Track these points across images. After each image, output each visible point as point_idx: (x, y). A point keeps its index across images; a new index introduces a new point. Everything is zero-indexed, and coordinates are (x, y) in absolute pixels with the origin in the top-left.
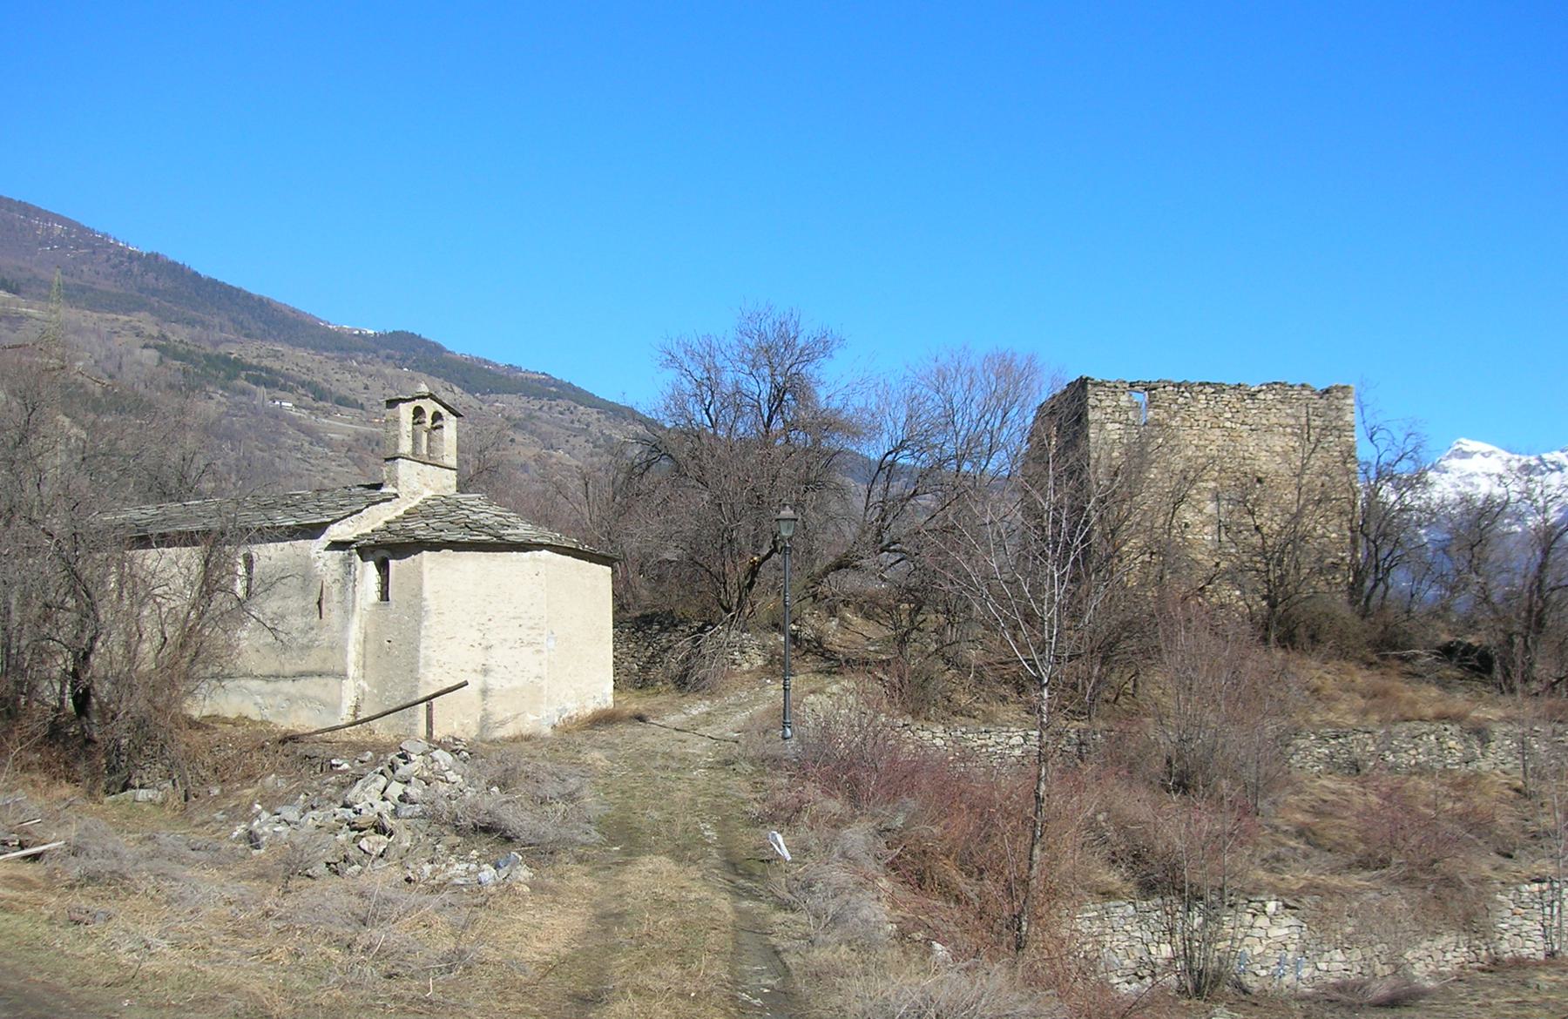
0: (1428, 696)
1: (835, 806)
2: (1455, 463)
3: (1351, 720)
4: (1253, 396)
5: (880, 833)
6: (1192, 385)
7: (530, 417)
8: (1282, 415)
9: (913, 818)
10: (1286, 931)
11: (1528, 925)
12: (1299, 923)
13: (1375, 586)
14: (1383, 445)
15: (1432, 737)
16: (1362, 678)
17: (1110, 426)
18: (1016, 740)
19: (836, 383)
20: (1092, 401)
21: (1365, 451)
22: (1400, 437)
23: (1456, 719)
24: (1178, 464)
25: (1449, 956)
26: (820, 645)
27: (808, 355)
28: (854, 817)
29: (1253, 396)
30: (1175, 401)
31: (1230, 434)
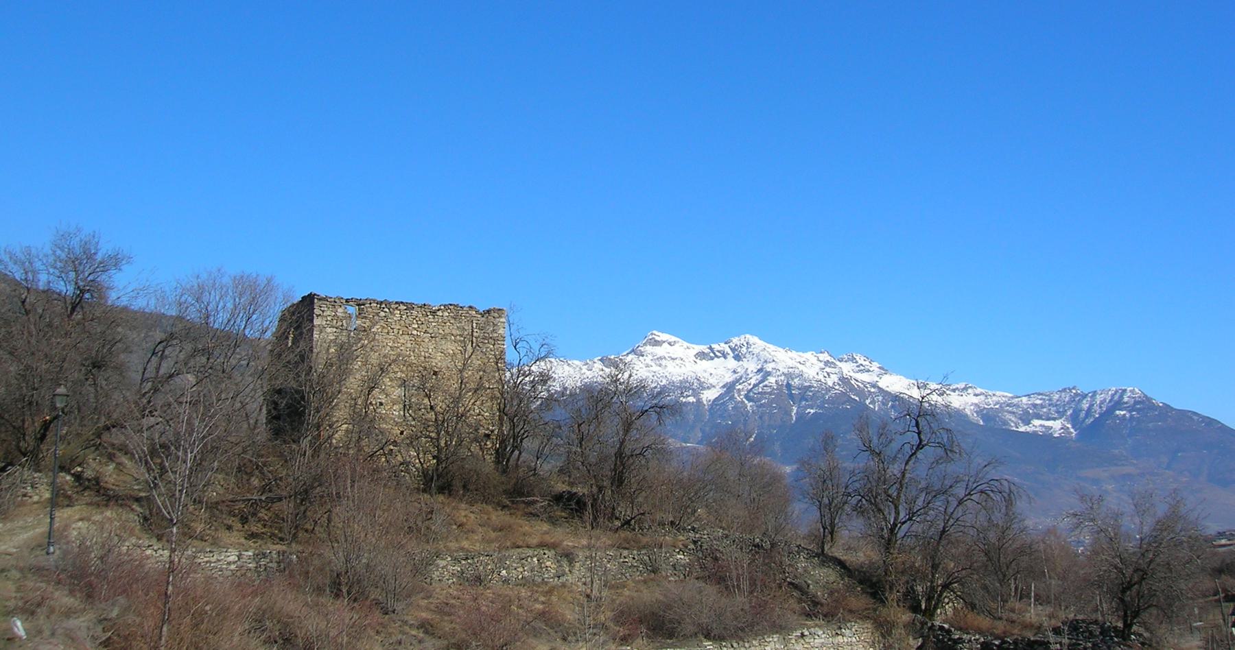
0: (539, 529)
1: (68, 601)
2: (649, 348)
3: (478, 547)
4: (434, 313)
5: (100, 621)
6: (390, 303)
8: (452, 328)
9: (126, 610)
16: (498, 517)
17: (329, 330)
18: (233, 558)
20: (317, 311)
21: (511, 356)
22: (536, 347)
23: (552, 546)
24: (374, 358)
26: (98, 483)
27: (104, 267)
28: (85, 610)
29: (434, 313)
30: (377, 314)
31: (417, 340)
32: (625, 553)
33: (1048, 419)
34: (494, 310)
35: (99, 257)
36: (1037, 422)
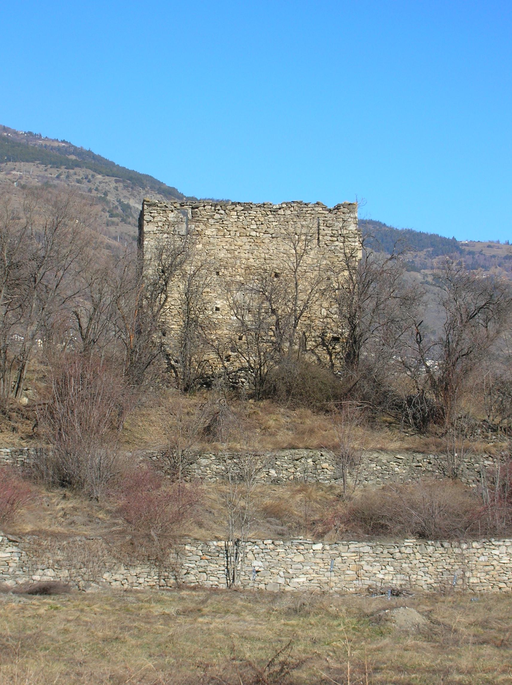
7: (47, 185)
10: (9, 555)
11: (212, 567)
12: (20, 550)
15: (310, 460)
25: (141, 580)
30: (212, 217)
32: (419, 457)
34: (344, 206)
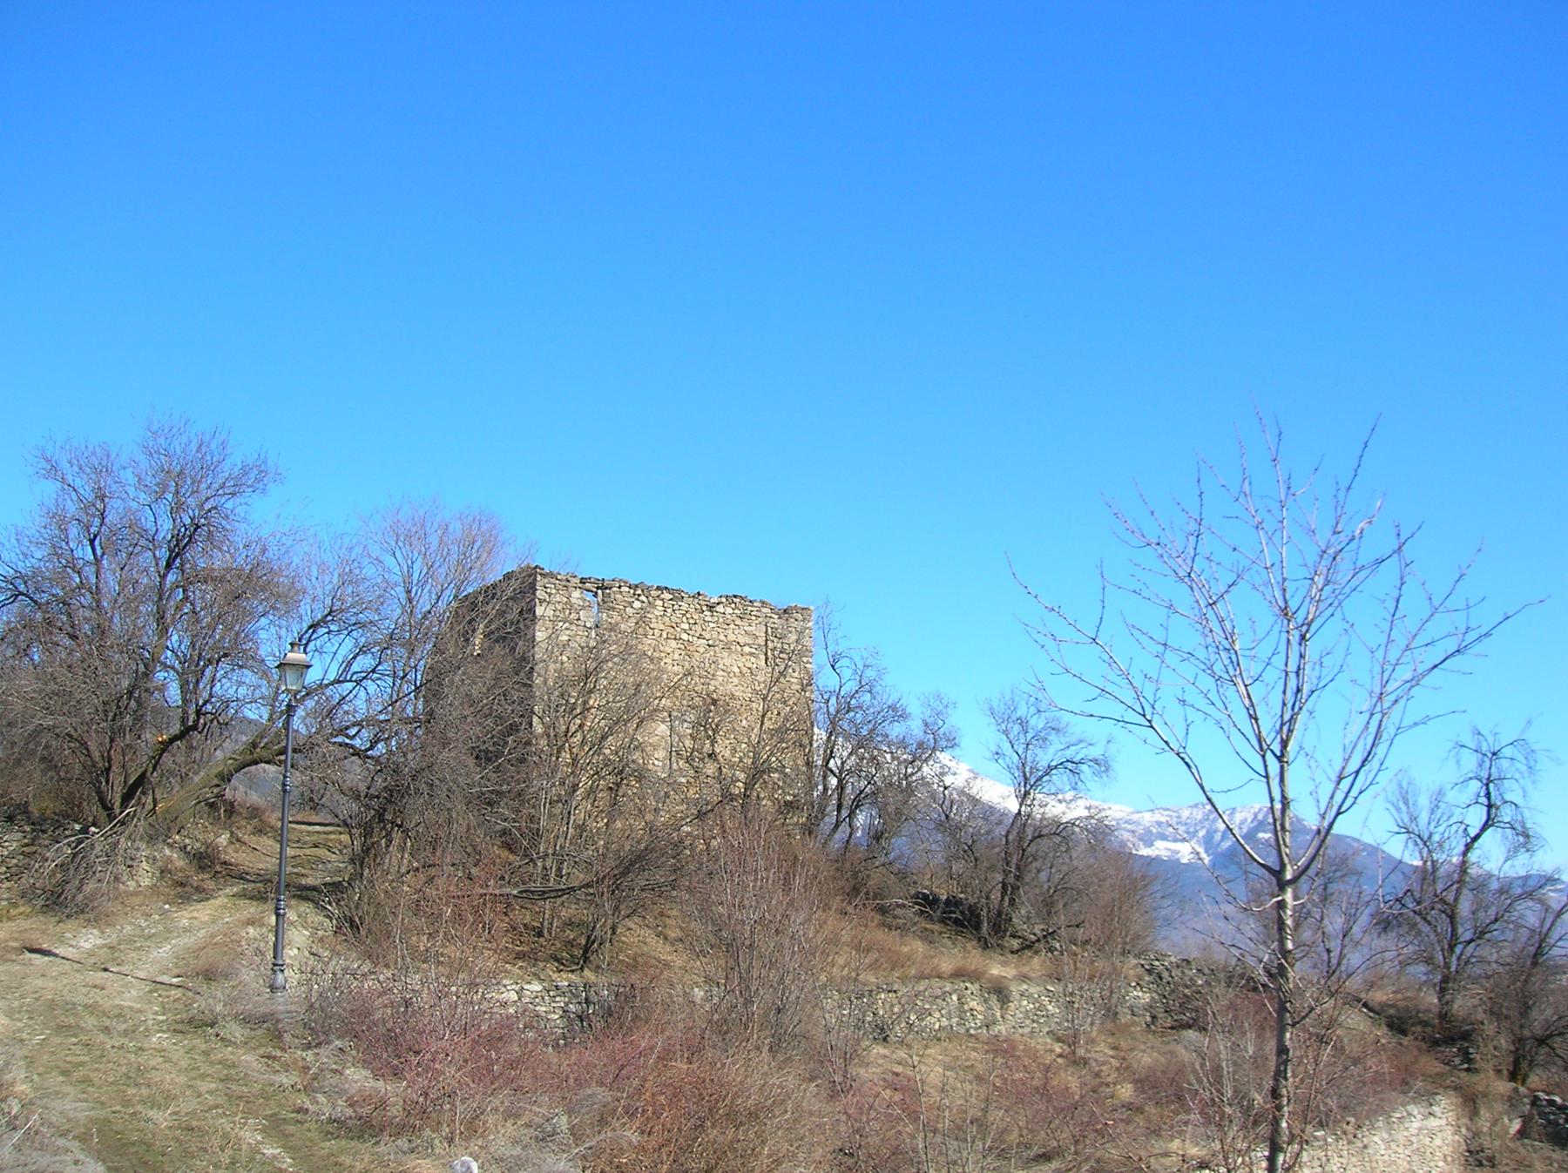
4: (711, 608)
13: (837, 826)
14: (847, 674)
15: (955, 997)
19: (260, 522)
20: (540, 594)
21: (827, 680)
29: (711, 608)
30: (631, 604)
33: (1175, 841)
35: (226, 470)
36: (1160, 844)
